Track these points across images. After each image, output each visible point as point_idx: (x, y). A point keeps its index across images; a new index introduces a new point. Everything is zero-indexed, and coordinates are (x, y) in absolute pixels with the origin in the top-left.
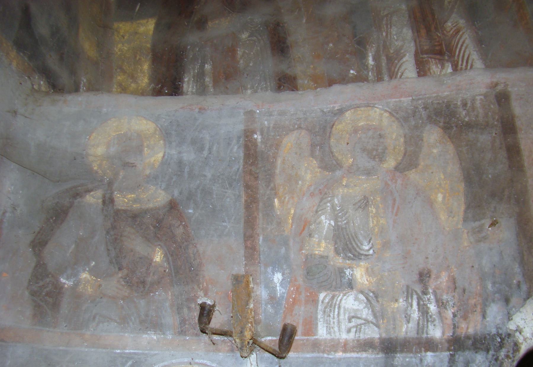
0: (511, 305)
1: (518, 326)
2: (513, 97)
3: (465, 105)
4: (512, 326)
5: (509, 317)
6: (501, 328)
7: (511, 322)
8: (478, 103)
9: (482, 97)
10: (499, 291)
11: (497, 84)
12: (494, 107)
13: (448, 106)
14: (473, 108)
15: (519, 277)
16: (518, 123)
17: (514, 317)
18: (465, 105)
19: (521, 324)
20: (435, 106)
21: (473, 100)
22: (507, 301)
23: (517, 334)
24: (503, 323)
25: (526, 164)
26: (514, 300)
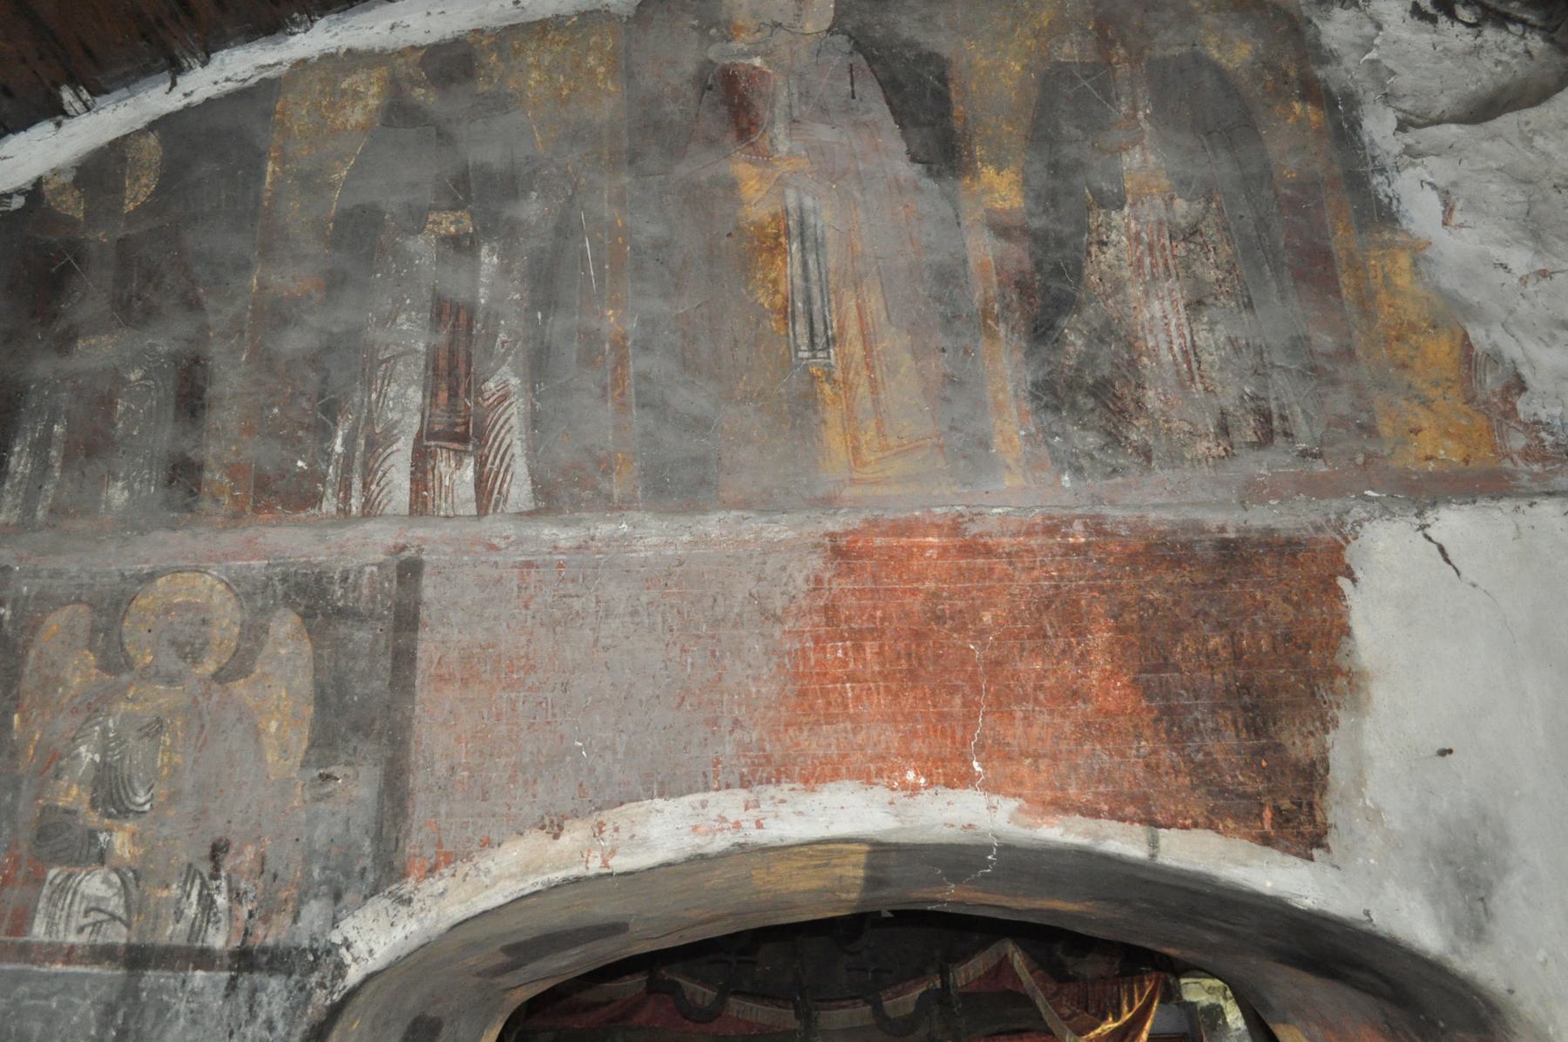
0: (341, 905)
1: (346, 939)
2: (427, 569)
3: (345, 579)
4: (336, 938)
5: (335, 923)
6: (316, 940)
7: (336, 932)
8: (365, 580)
9: (375, 569)
10: (328, 882)
11: (404, 548)
12: (392, 586)
13: (319, 579)
14: (356, 587)
15: (368, 862)
16: (423, 614)
17: (341, 924)
18: (345, 579)
19: (352, 935)
20: (299, 579)
21: (360, 572)
22: (337, 897)
23: (343, 951)
24: (323, 934)
25: (417, 682)
26: (348, 897)
